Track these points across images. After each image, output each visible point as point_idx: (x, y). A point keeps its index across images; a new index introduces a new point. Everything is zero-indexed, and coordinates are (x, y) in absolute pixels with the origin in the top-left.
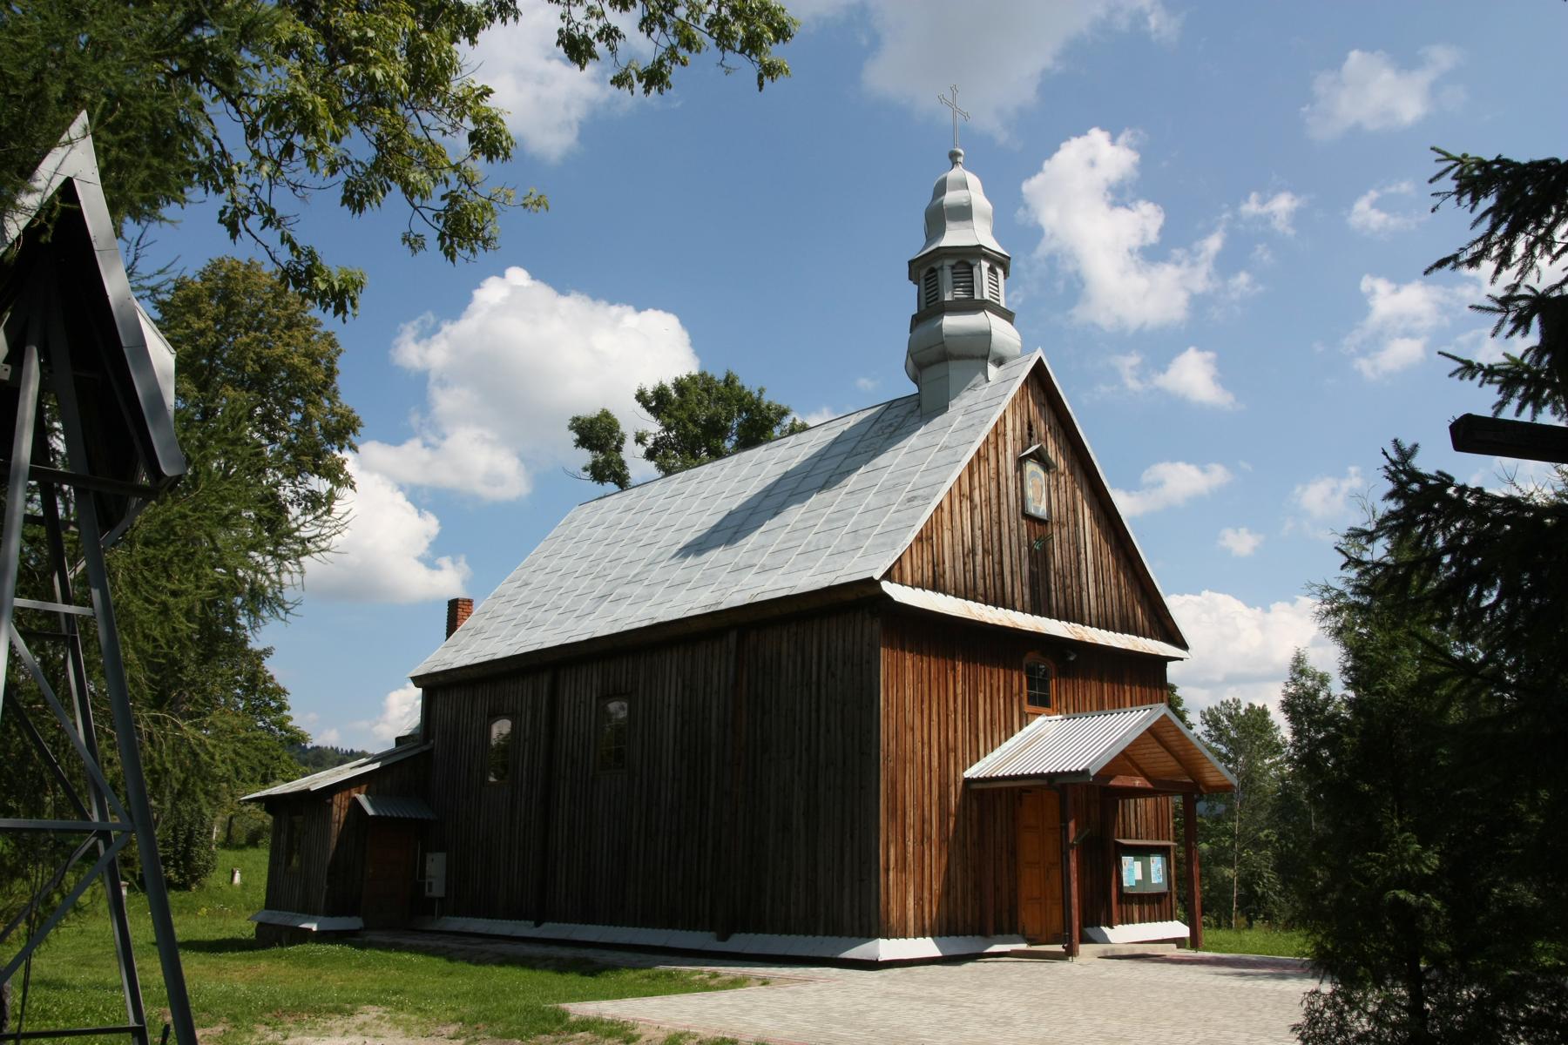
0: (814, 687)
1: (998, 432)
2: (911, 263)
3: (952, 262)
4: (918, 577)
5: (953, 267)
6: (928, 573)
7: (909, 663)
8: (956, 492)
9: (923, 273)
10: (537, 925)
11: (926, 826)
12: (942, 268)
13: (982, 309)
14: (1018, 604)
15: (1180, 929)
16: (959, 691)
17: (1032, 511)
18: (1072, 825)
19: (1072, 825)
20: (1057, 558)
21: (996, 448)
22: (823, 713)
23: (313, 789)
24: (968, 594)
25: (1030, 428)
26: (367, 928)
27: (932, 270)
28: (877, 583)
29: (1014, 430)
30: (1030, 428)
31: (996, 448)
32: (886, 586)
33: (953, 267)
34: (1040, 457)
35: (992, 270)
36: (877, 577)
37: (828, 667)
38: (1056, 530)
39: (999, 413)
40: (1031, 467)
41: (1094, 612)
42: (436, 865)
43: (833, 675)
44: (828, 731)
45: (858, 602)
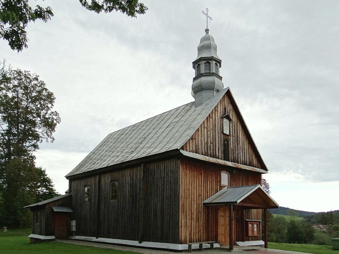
0: (163, 179)
1: (216, 109)
2: (193, 63)
3: (205, 62)
4: (191, 149)
5: (205, 63)
6: (194, 148)
7: (188, 172)
8: (203, 126)
9: (196, 65)
10: (97, 238)
11: (193, 215)
12: (202, 64)
13: (213, 75)
14: (220, 158)
15: (262, 243)
16: (202, 180)
17: (224, 132)
18: (24, 207)
19: (24, 207)
20: (231, 146)
21: (215, 114)
22: (165, 185)
23: (39, 205)
24: (206, 154)
25: (225, 109)
26: (56, 238)
27: (199, 65)
28: (179, 150)
29: (220, 110)
30: (225, 109)
31: (215, 114)
32: (181, 151)
33: (205, 63)
34: (228, 117)
35: (216, 64)
36: (179, 149)
37: (167, 173)
38: (231, 138)
39: (216, 104)
40: (225, 121)
41: (241, 160)
42: (74, 223)
43: (168, 175)
44: (166, 190)
45: (174, 155)
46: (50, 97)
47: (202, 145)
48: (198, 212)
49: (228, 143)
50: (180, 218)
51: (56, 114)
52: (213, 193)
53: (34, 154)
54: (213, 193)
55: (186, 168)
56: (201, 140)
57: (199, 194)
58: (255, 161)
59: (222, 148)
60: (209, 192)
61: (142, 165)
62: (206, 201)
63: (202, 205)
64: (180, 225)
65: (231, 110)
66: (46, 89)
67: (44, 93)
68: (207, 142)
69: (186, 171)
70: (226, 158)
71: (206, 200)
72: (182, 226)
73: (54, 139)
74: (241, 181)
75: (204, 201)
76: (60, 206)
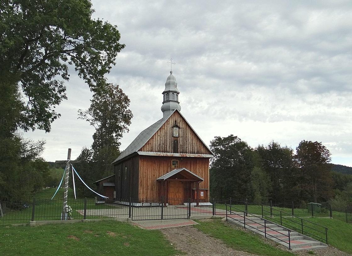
3: (166, 94)
24: (159, 151)
30: (176, 121)
46: (127, 100)
47: (155, 146)
48: (152, 185)
49: (177, 142)
50: (139, 189)
51: (130, 111)
52: (161, 175)
53: (119, 141)
54: (161, 175)
55: (144, 161)
56: (156, 143)
57: (153, 175)
58: (203, 150)
59: (173, 146)
60: (161, 173)
61: (131, 158)
62: (159, 178)
63: (156, 182)
64: (139, 193)
65: (181, 121)
66: (124, 94)
67: (123, 97)
68: (160, 144)
69: (144, 163)
70: (175, 151)
71: (158, 178)
72: (140, 193)
73: (129, 130)
74: (189, 166)
75: (157, 178)
76: (108, 182)
